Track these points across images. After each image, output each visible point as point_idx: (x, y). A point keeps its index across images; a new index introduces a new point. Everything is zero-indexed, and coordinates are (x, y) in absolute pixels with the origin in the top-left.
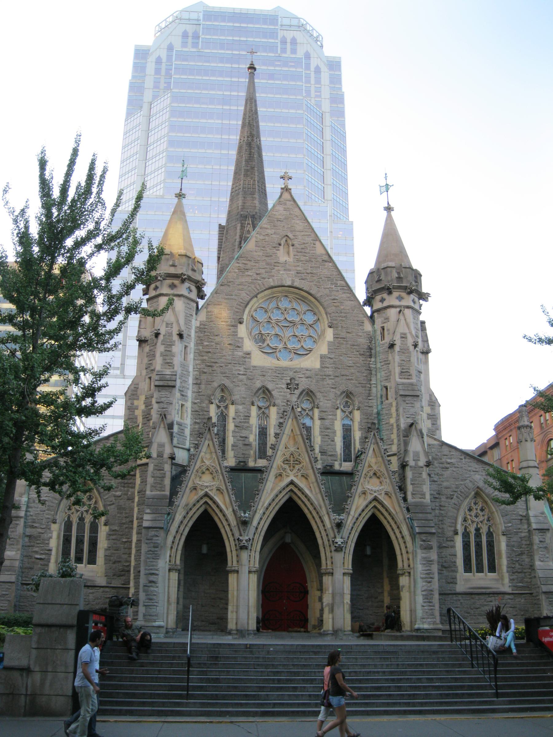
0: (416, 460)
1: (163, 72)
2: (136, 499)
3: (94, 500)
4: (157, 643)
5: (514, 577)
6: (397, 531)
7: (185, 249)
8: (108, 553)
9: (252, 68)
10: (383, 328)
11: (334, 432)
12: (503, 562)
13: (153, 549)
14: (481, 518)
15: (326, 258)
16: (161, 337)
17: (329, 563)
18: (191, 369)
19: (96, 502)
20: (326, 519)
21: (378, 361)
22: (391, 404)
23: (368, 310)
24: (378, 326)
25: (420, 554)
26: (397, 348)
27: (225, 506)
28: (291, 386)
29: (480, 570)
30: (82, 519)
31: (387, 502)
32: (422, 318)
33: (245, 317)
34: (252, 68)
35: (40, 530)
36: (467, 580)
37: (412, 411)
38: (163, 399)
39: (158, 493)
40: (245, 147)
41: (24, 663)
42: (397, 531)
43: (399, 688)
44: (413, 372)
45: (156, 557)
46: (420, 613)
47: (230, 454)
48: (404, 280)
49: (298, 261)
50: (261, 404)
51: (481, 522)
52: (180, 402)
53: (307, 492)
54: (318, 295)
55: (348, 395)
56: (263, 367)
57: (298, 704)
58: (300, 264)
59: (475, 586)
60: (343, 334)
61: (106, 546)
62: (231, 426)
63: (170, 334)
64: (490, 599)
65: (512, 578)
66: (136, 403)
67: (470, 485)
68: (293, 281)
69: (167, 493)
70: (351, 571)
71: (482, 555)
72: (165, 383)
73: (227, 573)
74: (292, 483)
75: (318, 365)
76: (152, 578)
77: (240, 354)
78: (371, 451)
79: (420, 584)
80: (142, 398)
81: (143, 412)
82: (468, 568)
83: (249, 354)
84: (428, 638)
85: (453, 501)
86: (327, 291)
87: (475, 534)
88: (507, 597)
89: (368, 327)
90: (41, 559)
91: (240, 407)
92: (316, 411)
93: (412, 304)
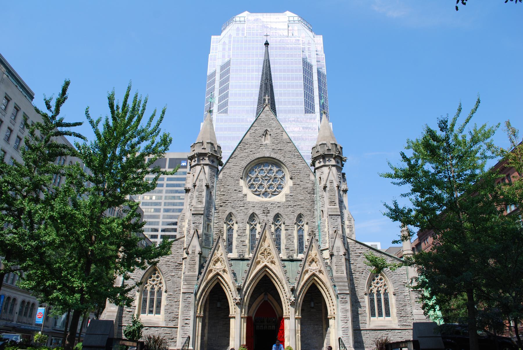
1: (227, 49)
2: (182, 277)
3: (160, 278)
5: (401, 319)
6: (327, 293)
7: (211, 139)
8: (167, 308)
9: (267, 44)
10: (320, 178)
12: (393, 310)
13: (187, 305)
16: (196, 188)
19: (161, 280)
20: (285, 286)
21: (318, 196)
22: (325, 220)
23: (313, 169)
24: (317, 177)
25: (341, 306)
26: (327, 189)
28: (266, 212)
29: (380, 315)
30: (153, 288)
31: (320, 276)
32: (343, 171)
34: (267, 44)
38: (196, 222)
39: (192, 273)
40: (264, 86)
42: (327, 293)
47: (234, 250)
48: (331, 151)
51: (381, 287)
52: (207, 223)
59: (377, 325)
61: (165, 304)
62: (235, 235)
63: (202, 186)
65: (400, 319)
66: (183, 223)
69: (197, 273)
70: (300, 317)
71: (381, 306)
72: (198, 212)
74: (266, 266)
75: (284, 200)
76: (187, 321)
80: (187, 221)
81: (187, 228)
82: (373, 315)
83: (246, 195)
87: (377, 294)
89: (312, 177)
90: (129, 312)
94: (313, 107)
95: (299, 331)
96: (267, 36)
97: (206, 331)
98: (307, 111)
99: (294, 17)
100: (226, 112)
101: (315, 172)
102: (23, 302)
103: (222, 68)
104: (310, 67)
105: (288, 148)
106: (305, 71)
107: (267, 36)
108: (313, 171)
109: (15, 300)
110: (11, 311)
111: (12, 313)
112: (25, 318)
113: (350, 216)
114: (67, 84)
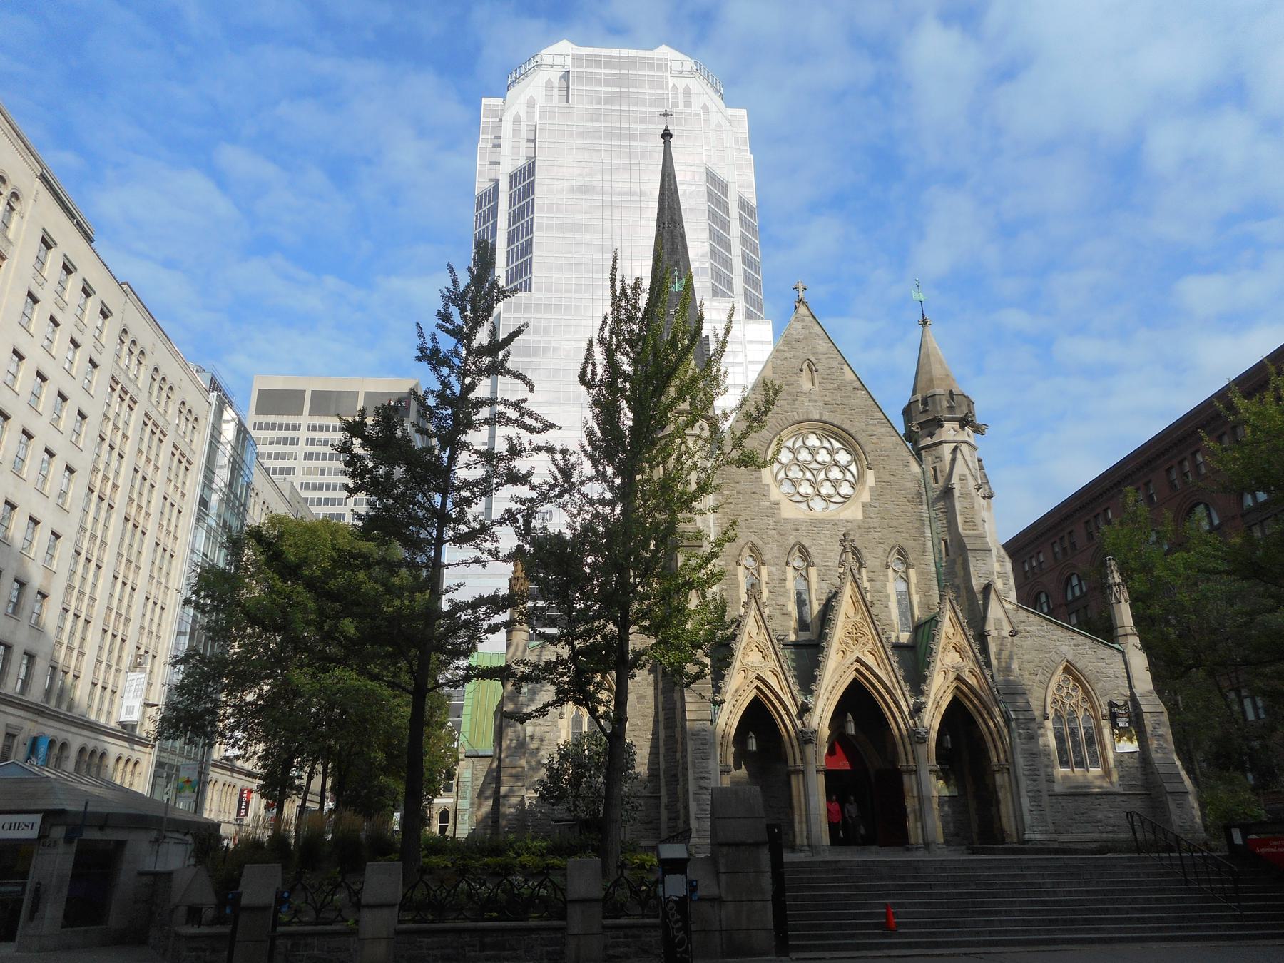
0: (999, 629)
4: (792, 863)
11: (887, 596)
14: (1074, 700)
15: (857, 384)
17: (910, 758)
18: (712, 525)
27: (785, 693)
35: (546, 729)
36: (1065, 778)
37: (985, 568)
41: (714, 891)
43: (1118, 911)
44: (978, 521)
45: (706, 756)
46: (1028, 819)
48: (957, 410)
49: (825, 389)
50: (796, 565)
53: (877, 671)
54: (852, 431)
55: (902, 553)
56: (797, 520)
57: (1076, 930)
58: (827, 393)
60: (887, 477)
64: (1097, 802)
67: (1058, 659)
68: (821, 414)
73: (789, 774)
77: (768, 504)
78: (947, 619)
79: (1024, 784)
84: (1075, 852)
85: (1037, 678)
86: (863, 426)
88: (1119, 798)
89: (915, 468)
91: (774, 569)
92: (813, 571)
93: (967, 439)
94: (729, 283)
95: (797, 818)
96: (666, 115)
99: (682, 62)
102: (82, 750)
103: (515, 178)
104: (723, 188)
106: (711, 197)
107: (666, 115)
109: (64, 746)
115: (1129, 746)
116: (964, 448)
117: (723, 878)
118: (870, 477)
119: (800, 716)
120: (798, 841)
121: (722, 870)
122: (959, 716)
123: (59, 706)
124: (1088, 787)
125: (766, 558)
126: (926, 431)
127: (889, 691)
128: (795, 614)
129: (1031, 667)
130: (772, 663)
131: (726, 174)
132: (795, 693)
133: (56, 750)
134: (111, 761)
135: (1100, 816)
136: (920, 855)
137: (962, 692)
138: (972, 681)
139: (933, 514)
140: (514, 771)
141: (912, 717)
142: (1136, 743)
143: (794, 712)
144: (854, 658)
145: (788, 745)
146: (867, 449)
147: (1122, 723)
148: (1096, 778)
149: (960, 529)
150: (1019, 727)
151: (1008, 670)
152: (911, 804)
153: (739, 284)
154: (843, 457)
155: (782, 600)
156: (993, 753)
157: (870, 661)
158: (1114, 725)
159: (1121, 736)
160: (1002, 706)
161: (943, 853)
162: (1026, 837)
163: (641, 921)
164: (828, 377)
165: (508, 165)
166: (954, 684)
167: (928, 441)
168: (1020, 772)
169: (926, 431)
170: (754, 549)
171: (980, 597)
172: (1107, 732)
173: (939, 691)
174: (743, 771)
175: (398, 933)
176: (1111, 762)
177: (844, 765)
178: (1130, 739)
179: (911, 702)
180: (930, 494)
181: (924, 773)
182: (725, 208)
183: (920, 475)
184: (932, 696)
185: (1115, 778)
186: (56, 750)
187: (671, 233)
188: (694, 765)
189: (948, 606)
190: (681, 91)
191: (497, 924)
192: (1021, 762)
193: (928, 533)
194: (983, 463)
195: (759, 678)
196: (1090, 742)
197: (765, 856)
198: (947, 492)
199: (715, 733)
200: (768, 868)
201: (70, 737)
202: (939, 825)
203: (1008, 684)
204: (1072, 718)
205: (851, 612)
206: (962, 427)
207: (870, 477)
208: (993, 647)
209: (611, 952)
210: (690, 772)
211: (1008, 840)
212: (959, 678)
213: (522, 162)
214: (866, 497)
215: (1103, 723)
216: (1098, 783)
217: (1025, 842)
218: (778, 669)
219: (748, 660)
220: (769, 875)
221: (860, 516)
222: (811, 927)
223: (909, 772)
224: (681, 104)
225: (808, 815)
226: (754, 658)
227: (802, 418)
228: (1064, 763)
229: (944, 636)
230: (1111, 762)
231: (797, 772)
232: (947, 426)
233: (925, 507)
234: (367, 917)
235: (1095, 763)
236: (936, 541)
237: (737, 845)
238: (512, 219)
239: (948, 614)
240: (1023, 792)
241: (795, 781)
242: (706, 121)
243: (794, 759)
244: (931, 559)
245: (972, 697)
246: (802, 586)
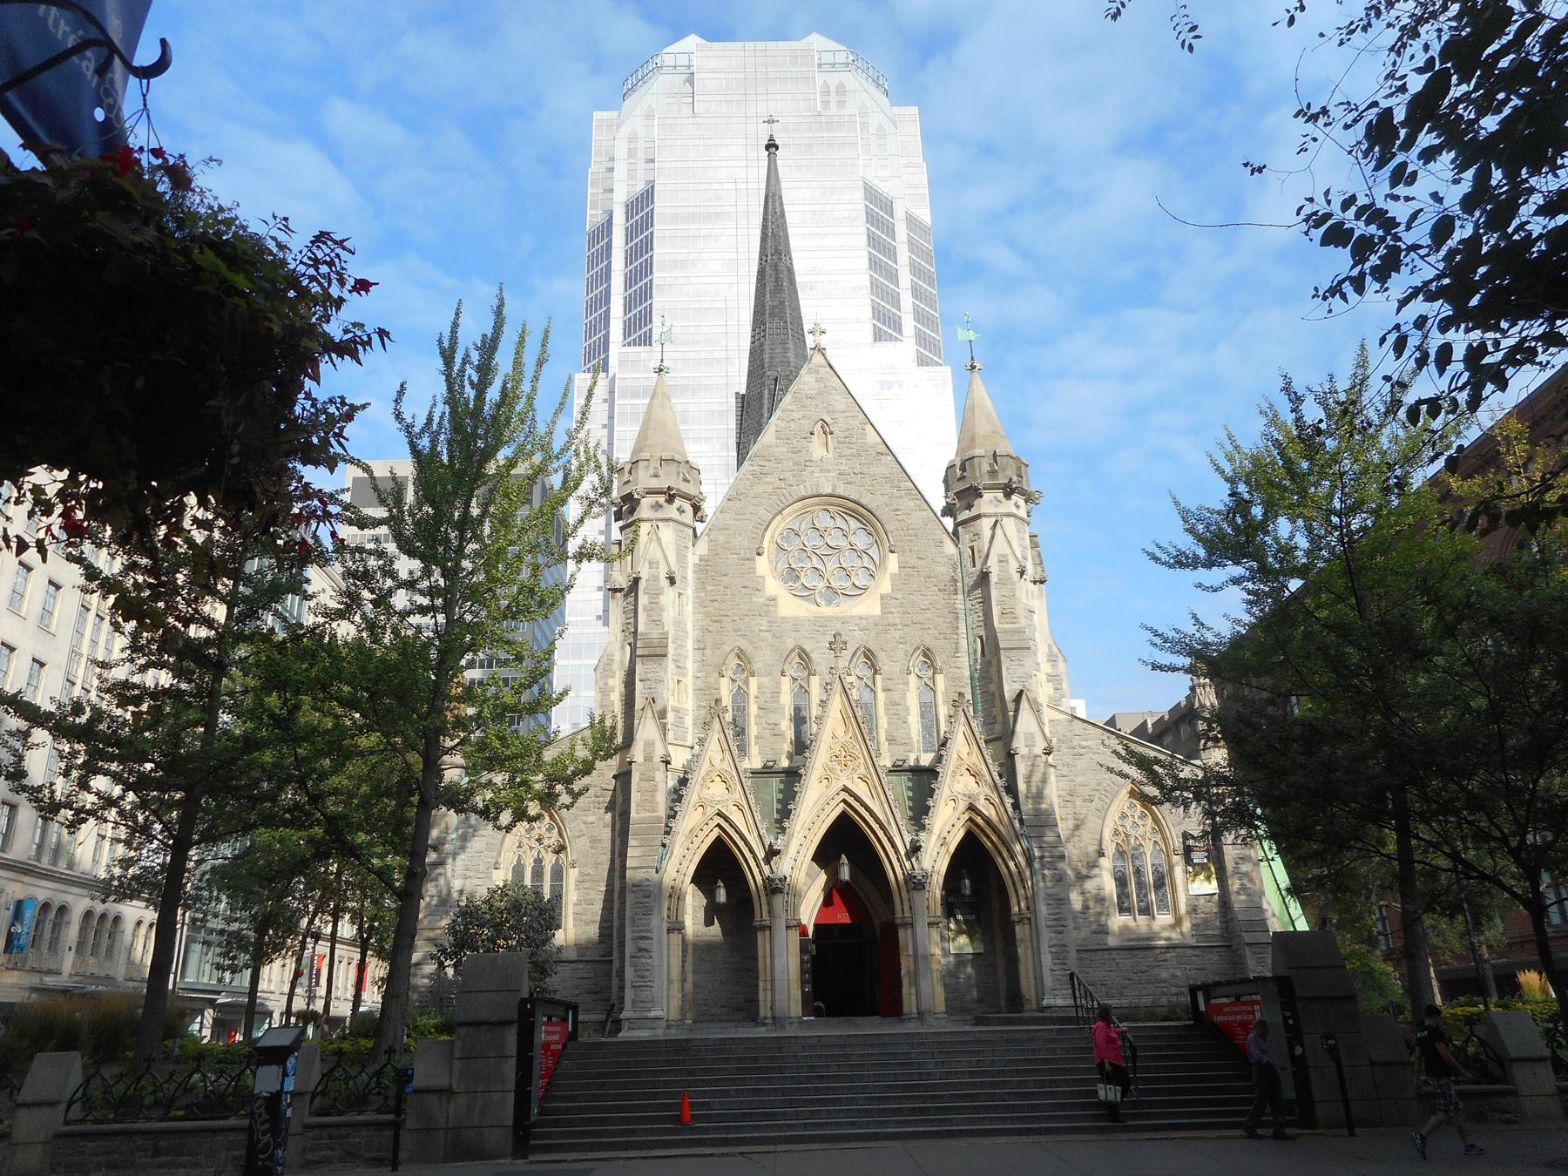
0: (1030, 746)
9: (771, 146)
11: (907, 709)
17: (906, 908)
18: (689, 627)
23: (949, 522)
27: (751, 835)
33: (766, 544)
34: (771, 146)
35: (478, 882)
36: (1125, 929)
37: (1020, 671)
41: (443, 1081)
45: (648, 912)
47: (754, 750)
48: (1000, 475)
54: (872, 506)
55: (927, 653)
58: (843, 460)
60: (913, 561)
68: (834, 487)
78: (960, 737)
79: (1047, 937)
89: (950, 548)
91: (765, 680)
93: (1014, 510)
94: (897, 325)
95: (761, 984)
97: (689, 967)
98: (878, 336)
99: (834, 52)
100: (646, 340)
101: (956, 533)
102: (88, 914)
104: (888, 207)
105: (884, 467)
106: (871, 218)
108: (950, 530)
109: (63, 910)
110: (54, 944)
111: (55, 951)
112: (92, 960)
113: (1055, 650)
114: (1194, 616)
115: (1206, 887)
116: (1007, 522)
117: (457, 1064)
118: (893, 562)
119: (768, 860)
120: (762, 1014)
121: (457, 1055)
122: (974, 859)
123: (54, 862)
124: (1152, 939)
125: (755, 667)
126: (965, 502)
127: (882, 827)
128: (790, 734)
129: (1086, 791)
130: (738, 795)
131: (887, 188)
132: (763, 832)
133: (52, 915)
134: (128, 926)
135: (1164, 975)
136: (911, 1027)
137: (977, 825)
138: (990, 812)
139: (969, 605)
140: (431, 934)
141: (909, 858)
142: (1214, 883)
143: (761, 855)
144: (840, 786)
145: (755, 896)
146: (889, 527)
147: (1198, 857)
148: (1164, 928)
149: (996, 624)
150: (1043, 866)
151: (1039, 796)
152: (906, 964)
153: (909, 324)
154: (861, 540)
155: (773, 718)
156: (1013, 901)
157: (861, 790)
158: (1188, 860)
159: (1196, 875)
160: (1025, 844)
161: (940, 1024)
162: (1045, 1002)
163: (116, 1126)
164: (846, 441)
165: (621, 197)
166: (966, 816)
167: (966, 515)
168: (1042, 924)
169: (965, 502)
170: (741, 655)
171: (1011, 706)
172: (1179, 872)
173: (945, 827)
174: (716, 929)
175: (58, 1136)
176: (1183, 908)
177: (844, 918)
178: (1208, 878)
179: (908, 839)
180: (966, 580)
181: (921, 928)
182: (890, 230)
183: (956, 557)
184: (936, 831)
185: (1186, 926)
186: (52, 915)
187: (775, 267)
188: (633, 924)
189: (963, 719)
190: (833, 88)
191: (1473, 1087)
192: (1043, 909)
193: (962, 629)
194: (1039, 539)
195: (720, 814)
196: (1160, 884)
197: (511, 1037)
198: (984, 577)
199: (661, 883)
200: (514, 1052)
201: (69, 898)
202: (940, 991)
203: (1038, 813)
204: (1137, 855)
205: (840, 731)
206: (1008, 496)
207: (893, 562)
208: (1021, 769)
209: (309, 1156)
210: (628, 930)
211: (1027, 1007)
212: (971, 808)
213: (640, 187)
214: (885, 586)
215: (1176, 859)
216: (1165, 934)
217: (1042, 1009)
218: (744, 803)
219: (706, 794)
220: (512, 1062)
221: (877, 611)
222: (591, 1121)
223: (905, 925)
224: (833, 104)
225: (773, 981)
226: (717, 789)
227: (810, 493)
228: (1123, 909)
229: (955, 756)
230: (1183, 908)
231: (763, 928)
232: (988, 496)
233: (960, 596)
234: (23, 1116)
235: (1163, 906)
236: (971, 639)
237: (478, 1024)
238: (630, 257)
239: (962, 728)
240: (1044, 947)
241: (762, 940)
242: (864, 125)
243: (761, 913)
244: (964, 662)
245: (989, 831)
246: (928, 698)
